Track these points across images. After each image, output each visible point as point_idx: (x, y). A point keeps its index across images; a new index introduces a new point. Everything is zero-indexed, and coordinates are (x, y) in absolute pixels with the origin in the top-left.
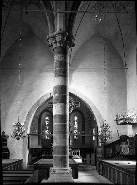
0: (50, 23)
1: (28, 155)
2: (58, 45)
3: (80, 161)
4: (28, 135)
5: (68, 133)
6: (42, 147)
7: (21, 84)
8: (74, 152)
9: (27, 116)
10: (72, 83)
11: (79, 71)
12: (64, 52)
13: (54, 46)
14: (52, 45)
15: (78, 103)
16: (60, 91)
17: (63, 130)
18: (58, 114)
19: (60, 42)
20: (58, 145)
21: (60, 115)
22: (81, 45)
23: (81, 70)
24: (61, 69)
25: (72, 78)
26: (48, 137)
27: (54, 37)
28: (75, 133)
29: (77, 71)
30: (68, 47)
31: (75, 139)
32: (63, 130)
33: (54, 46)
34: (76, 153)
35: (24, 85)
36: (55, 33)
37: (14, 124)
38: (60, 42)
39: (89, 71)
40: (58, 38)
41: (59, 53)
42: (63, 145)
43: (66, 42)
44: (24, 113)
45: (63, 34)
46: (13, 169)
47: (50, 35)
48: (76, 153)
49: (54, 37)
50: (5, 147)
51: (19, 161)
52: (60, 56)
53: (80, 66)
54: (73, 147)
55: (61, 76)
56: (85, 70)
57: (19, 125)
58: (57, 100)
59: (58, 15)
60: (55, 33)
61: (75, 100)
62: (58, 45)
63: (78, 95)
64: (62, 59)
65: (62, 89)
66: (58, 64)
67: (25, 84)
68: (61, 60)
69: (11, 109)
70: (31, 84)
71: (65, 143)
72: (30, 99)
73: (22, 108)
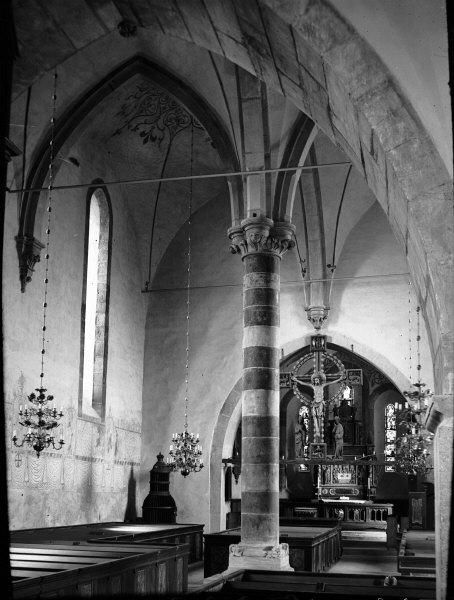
0: (233, 193)
1: (228, 515)
2: (251, 250)
3: (382, 536)
4: (225, 461)
5: (277, 459)
6: (290, 495)
7: (206, 329)
8: (373, 512)
9: (222, 411)
10: (342, 319)
11: (359, 285)
12: (265, 265)
13: (243, 254)
14: (239, 250)
15: (358, 373)
16: (256, 360)
17: (262, 453)
18: (252, 414)
19: (255, 244)
20: (249, 488)
21: (255, 417)
22: (365, 210)
23: (367, 280)
24: (257, 308)
25: (340, 303)
26: (306, 466)
27: (242, 232)
28: (389, 453)
29: (355, 284)
30: (277, 252)
31: (389, 473)
32: (262, 453)
33: (243, 254)
34: (379, 512)
35: (213, 330)
36: (243, 222)
37: (175, 436)
38: (255, 244)
39: (388, 283)
40: (250, 236)
41: (255, 270)
42: (263, 488)
43: (269, 241)
44: (214, 404)
45: (260, 224)
46: (314, 571)
47: (234, 226)
48: (379, 512)
49: (242, 232)
50: (164, 494)
51: (184, 529)
52: (255, 276)
53: (365, 270)
54: (378, 496)
55: (258, 324)
56: (380, 279)
57: (187, 439)
58: (248, 380)
59: (248, 179)
60: (243, 222)
61: (348, 365)
62: (251, 250)
63: (358, 351)
64: (261, 284)
65: (261, 356)
66: (251, 295)
67: (214, 328)
68: (258, 286)
69: (180, 395)
70: (232, 326)
71: (268, 483)
72: (228, 365)
73: (209, 390)
